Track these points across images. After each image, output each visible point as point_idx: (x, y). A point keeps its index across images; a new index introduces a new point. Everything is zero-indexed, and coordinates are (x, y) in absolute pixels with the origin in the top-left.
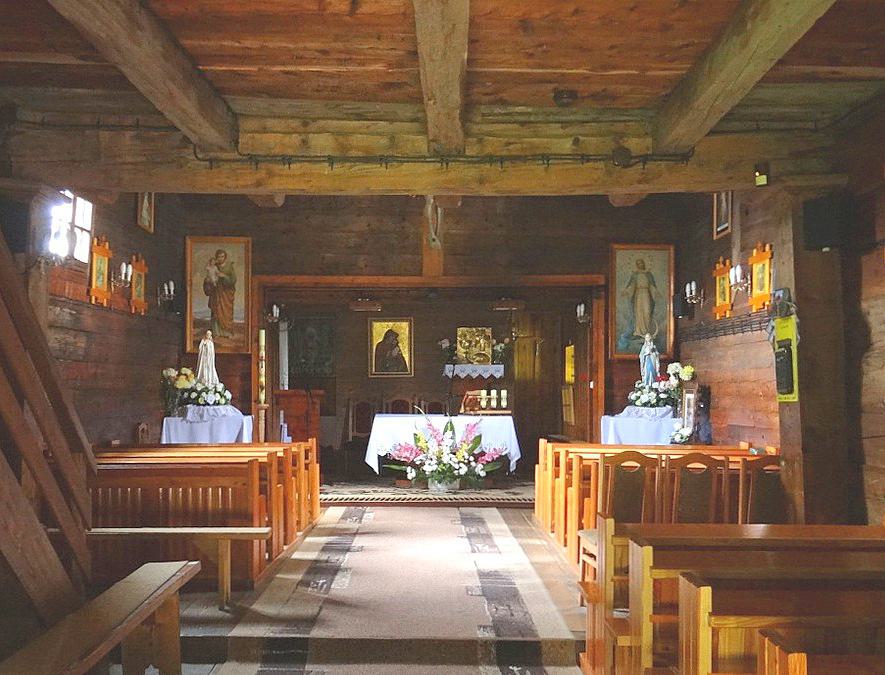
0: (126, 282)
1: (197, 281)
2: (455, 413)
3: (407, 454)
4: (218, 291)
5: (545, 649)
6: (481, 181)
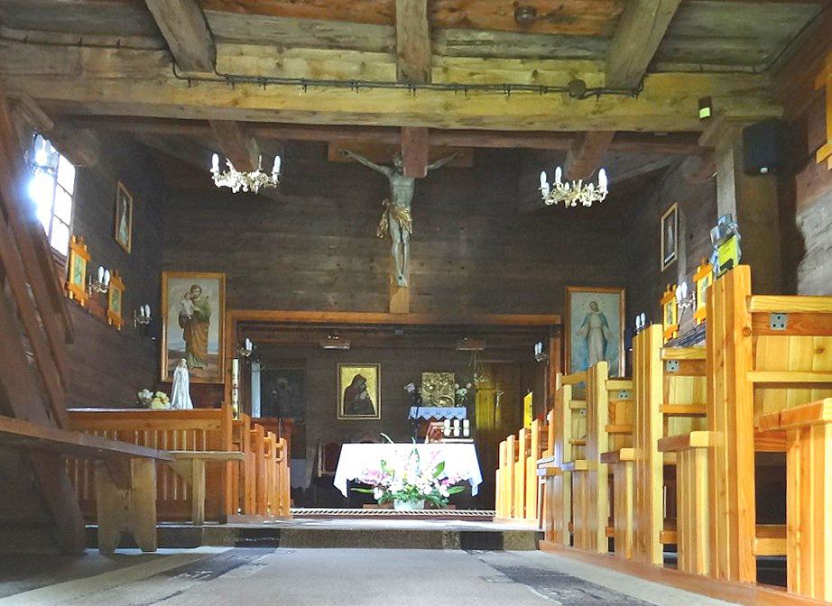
0: (103, 288)
1: (172, 315)
2: (421, 440)
3: (374, 478)
4: (193, 324)
5: (506, 538)
6: (447, 107)
